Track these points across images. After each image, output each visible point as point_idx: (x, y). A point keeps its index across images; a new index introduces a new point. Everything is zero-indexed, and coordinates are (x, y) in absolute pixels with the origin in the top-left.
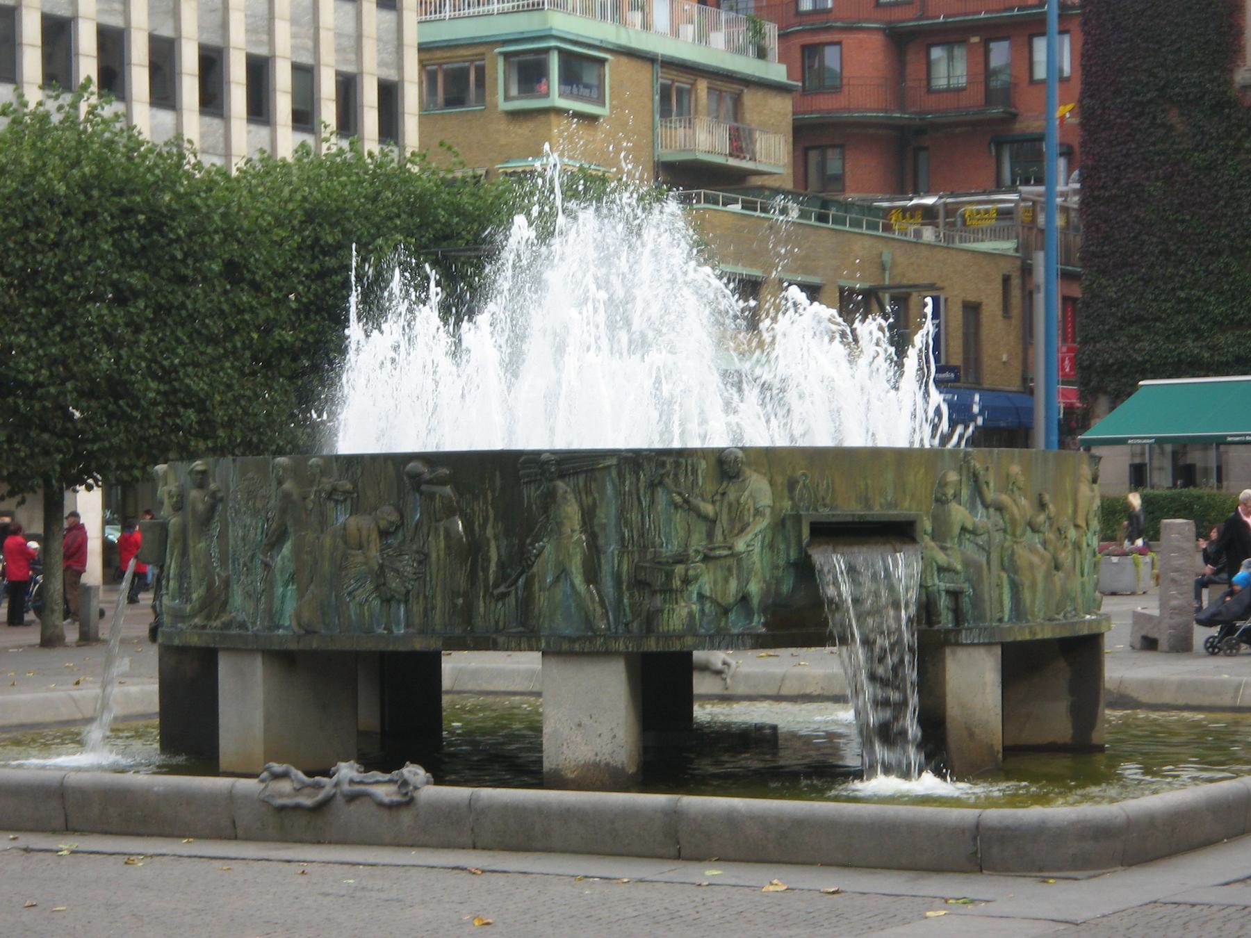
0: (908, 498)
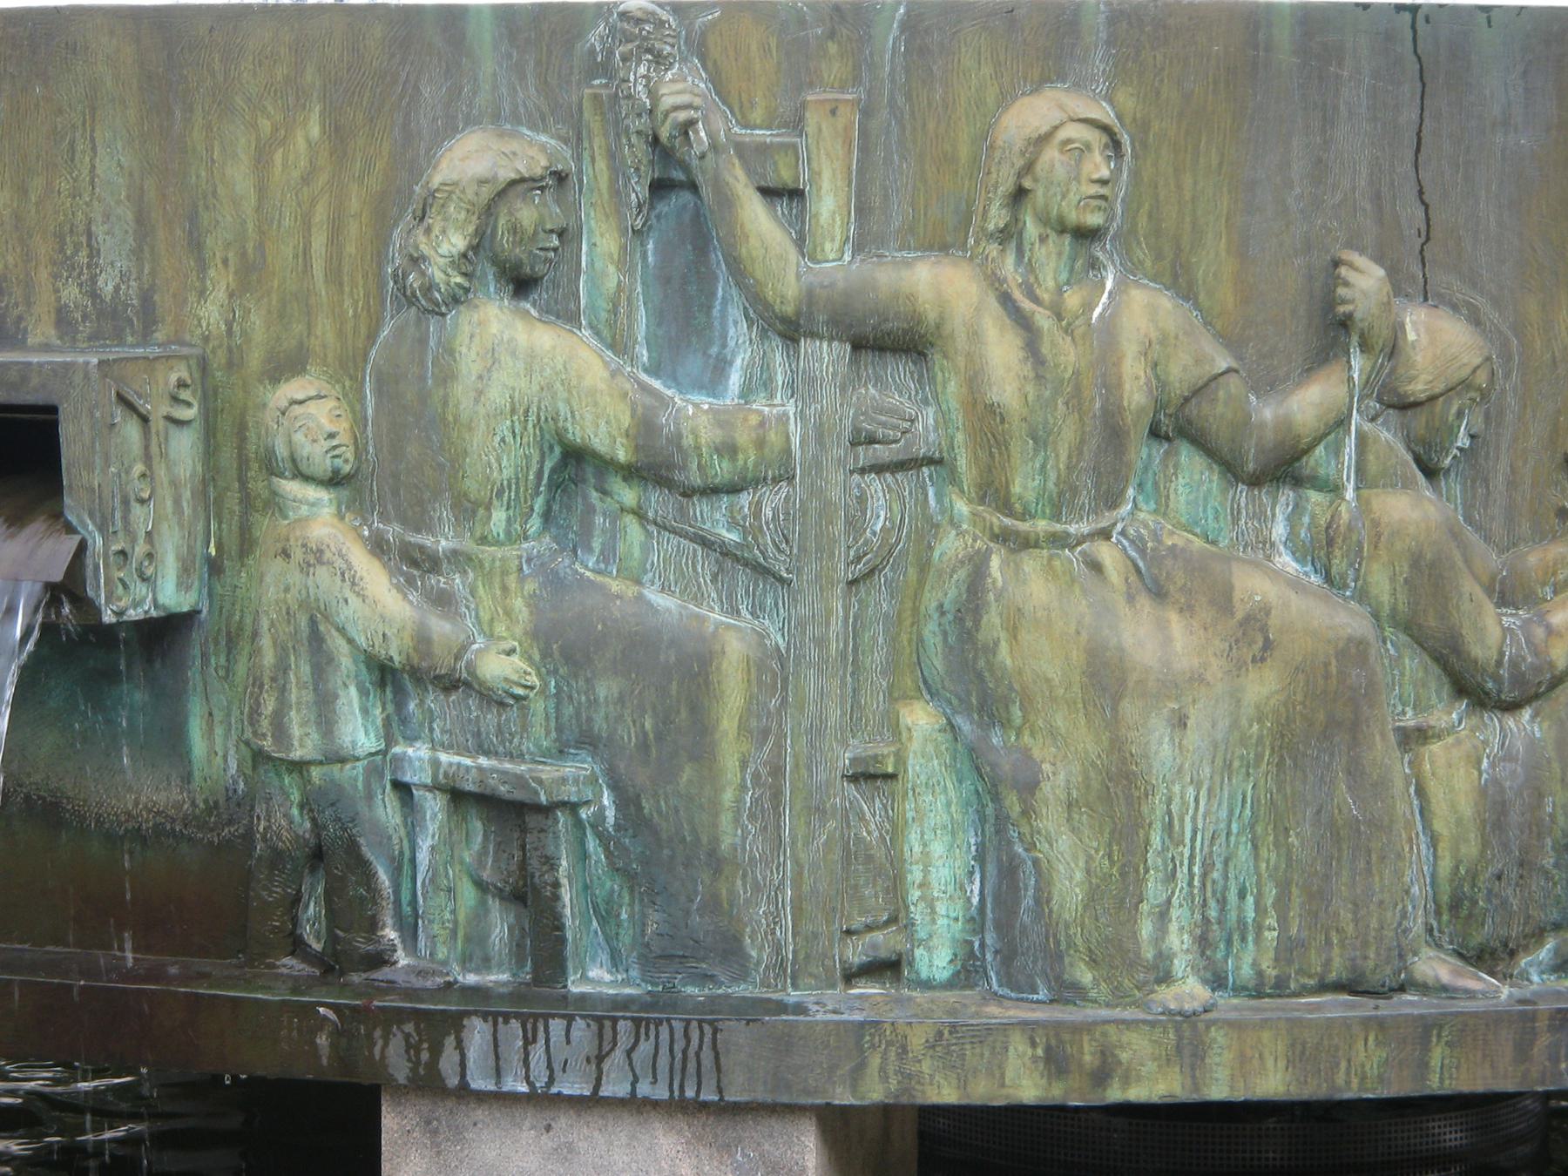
0: (220, 283)
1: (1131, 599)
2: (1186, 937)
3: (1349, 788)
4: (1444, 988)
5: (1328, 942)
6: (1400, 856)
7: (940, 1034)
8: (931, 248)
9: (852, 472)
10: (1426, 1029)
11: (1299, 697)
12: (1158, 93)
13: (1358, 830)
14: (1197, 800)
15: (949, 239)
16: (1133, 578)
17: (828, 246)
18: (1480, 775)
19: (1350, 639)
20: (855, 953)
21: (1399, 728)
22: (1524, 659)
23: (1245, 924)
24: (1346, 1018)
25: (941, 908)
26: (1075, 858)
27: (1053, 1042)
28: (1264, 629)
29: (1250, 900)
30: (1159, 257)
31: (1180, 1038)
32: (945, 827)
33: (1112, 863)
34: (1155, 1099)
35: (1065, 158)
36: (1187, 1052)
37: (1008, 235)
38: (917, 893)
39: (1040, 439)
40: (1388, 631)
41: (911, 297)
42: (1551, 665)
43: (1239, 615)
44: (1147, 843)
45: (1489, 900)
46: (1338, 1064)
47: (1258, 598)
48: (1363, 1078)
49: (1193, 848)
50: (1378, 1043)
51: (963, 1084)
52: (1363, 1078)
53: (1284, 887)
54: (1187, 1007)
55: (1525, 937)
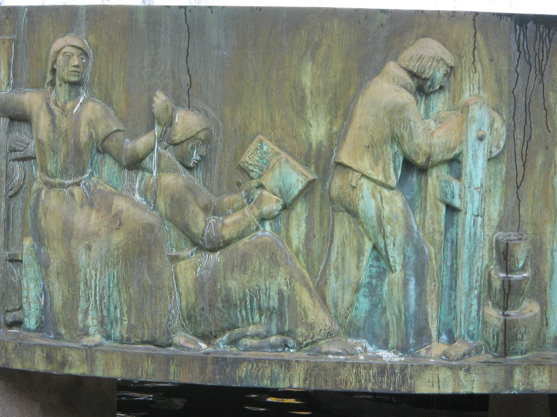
1: (82, 206)
2: (95, 321)
3: (148, 275)
4: (181, 346)
5: (143, 326)
6: (166, 299)
7: (16, 346)
8: (34, 88)
9: (10, 161)
10: (169, 359)
11: (130, 242)
12: (101, 37)
13: (152, 289)
14: (96, 275)
15: (39, 85)
16: (84, 199)
17: (3, 87)
18: (196, 273)
19: (147, 224)
20: (10, 318)
21: (170, 255)
22: (212, 234)
23: (117, 318)
24: (141, 353)
25: (32, 305)
26: (59, 291)
27: (49, 352)
28: (120, 219)
29: (118, 310)
30: (101, 92)
31: (87, 354)
32: (34, 279)
33: (69, 294)
34: (79, 374)
35: (64, 58)
36: (89, 359)
37: (53, 83)
38: (25, 300)
39: (55, 152)
40: (166, 222)
41: (22, 104)
42: (223, 237)
43: (113, 213)
44: (79, 288)
45: (201, 317)
46: (139, 369)
47: (120, 208)
48: (147, 374)
49: (95, 291)
50: (152, 363)
51: (23, 363)
52: (147, 374)
53: (129, 307)
54: (89, 344)
55: (218, 331)
